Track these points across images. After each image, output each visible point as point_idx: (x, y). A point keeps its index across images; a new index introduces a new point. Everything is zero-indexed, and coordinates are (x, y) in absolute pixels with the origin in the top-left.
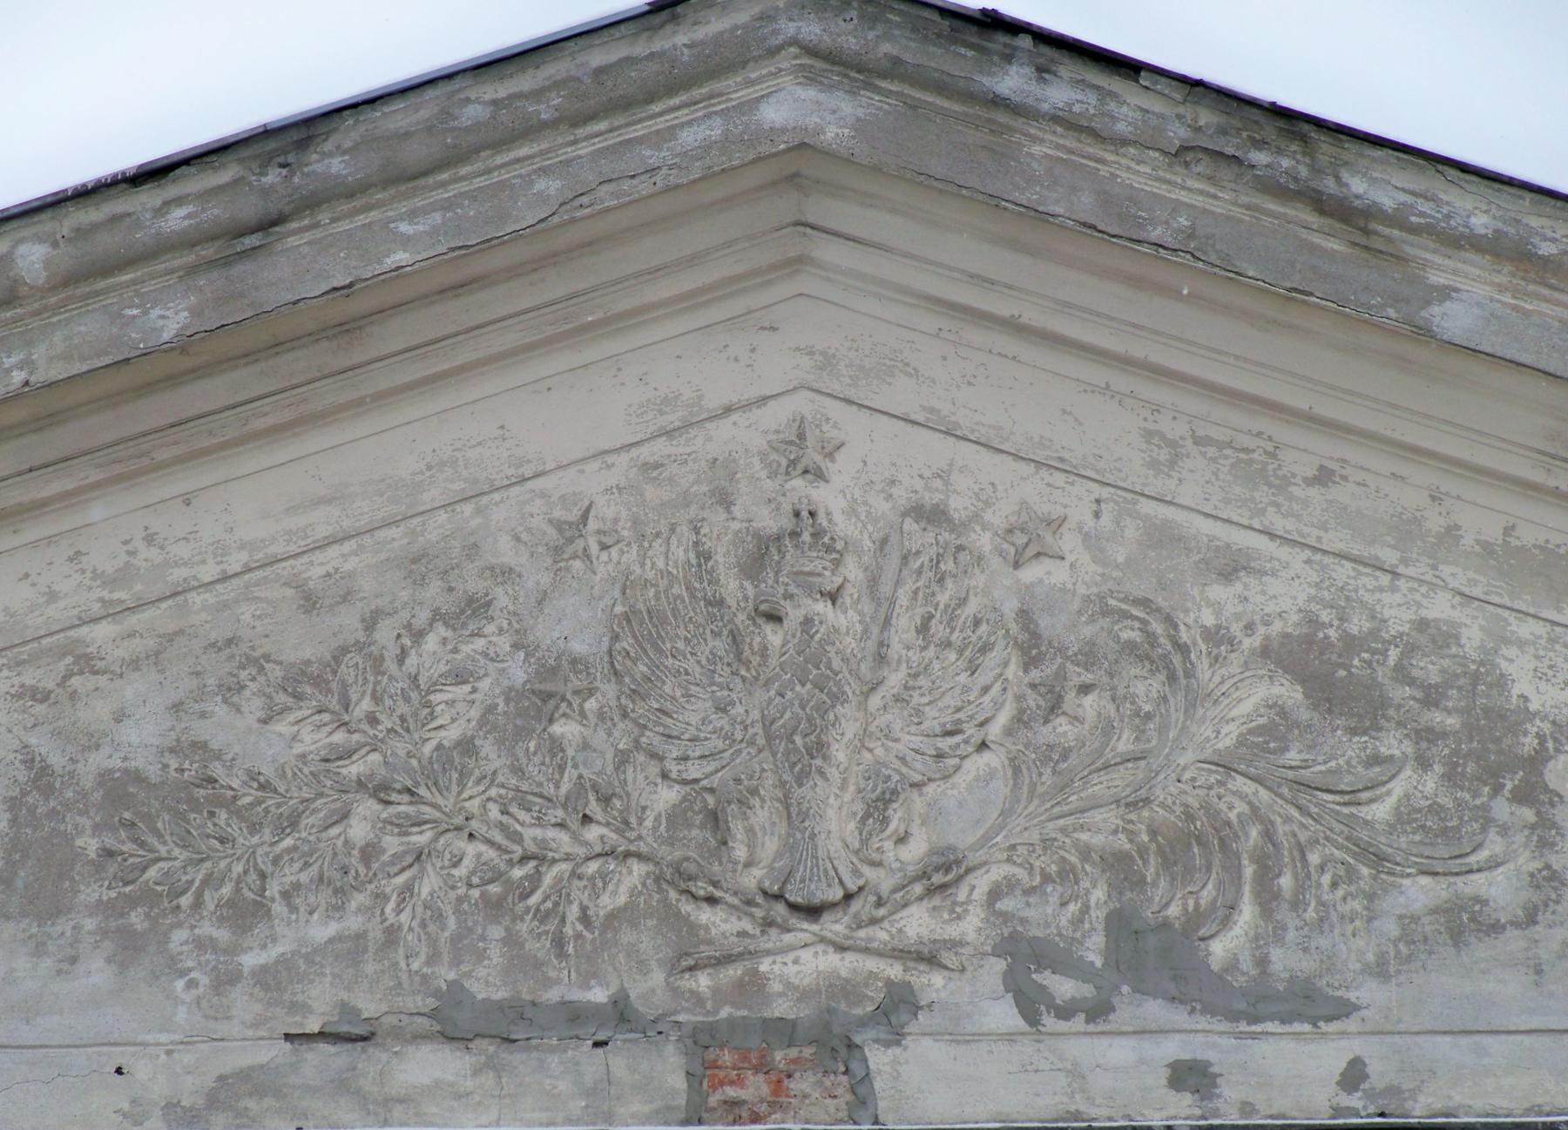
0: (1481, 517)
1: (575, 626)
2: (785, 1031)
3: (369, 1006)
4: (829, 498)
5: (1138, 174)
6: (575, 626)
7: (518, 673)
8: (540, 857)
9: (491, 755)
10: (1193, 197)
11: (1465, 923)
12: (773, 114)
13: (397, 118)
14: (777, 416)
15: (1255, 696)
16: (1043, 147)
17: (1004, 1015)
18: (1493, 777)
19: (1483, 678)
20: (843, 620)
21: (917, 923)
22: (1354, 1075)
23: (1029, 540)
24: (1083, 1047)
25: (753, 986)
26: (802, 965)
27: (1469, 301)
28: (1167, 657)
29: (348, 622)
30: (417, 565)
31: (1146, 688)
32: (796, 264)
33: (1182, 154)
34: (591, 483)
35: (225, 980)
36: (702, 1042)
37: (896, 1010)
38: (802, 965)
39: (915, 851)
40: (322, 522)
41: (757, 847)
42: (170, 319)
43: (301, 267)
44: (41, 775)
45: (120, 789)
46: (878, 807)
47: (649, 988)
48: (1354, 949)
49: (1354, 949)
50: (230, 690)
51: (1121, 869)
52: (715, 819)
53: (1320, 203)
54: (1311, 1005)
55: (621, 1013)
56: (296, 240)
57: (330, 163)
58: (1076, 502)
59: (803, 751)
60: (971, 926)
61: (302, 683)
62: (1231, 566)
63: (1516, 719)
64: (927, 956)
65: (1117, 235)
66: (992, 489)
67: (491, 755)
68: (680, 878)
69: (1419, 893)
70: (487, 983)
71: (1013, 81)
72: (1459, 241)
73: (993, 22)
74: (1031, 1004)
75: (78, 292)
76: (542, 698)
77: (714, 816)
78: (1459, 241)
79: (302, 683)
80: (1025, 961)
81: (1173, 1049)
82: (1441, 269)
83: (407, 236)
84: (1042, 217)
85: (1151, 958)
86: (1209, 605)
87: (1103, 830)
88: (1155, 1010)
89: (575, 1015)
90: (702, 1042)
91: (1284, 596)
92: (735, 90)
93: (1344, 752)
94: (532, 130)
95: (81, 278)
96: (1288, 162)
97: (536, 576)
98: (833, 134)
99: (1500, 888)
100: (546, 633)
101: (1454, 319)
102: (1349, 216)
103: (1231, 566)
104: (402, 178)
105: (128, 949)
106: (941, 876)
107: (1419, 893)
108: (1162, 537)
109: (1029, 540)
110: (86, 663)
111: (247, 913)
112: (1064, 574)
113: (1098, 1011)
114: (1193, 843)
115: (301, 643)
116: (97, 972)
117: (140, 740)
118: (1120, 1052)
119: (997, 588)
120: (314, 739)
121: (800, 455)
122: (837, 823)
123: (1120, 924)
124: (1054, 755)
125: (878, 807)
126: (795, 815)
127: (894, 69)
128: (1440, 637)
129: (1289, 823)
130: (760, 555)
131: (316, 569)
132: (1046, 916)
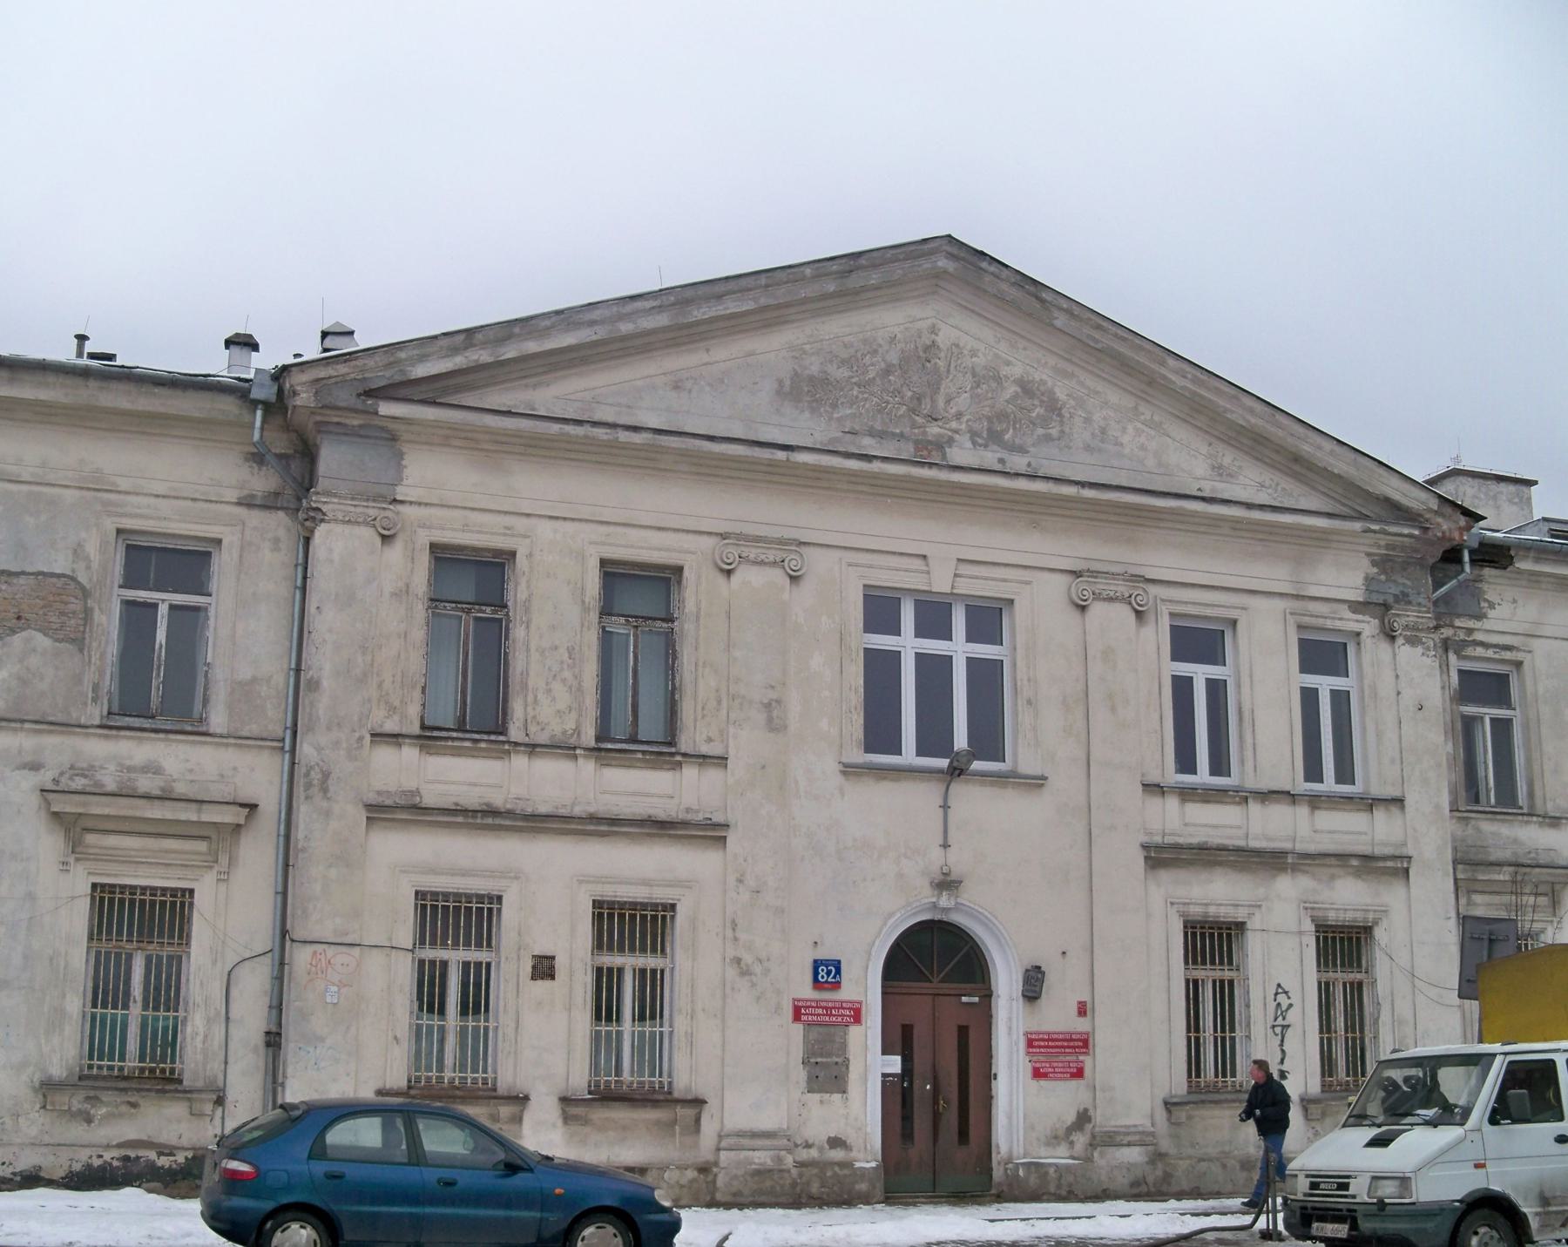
0: (1052, 361)
1: (893, 357)
2: (930, 442)
3: (857, 428)
4: (939, 339)
5: (1004, 286)
6: (893, 357)
7: (883, 365)
8: (887, 402)
9: (878, 381)
10: (1014, 293)
11: (1048, 438)
12: (940, 264)
13: (875, 254)
14: (929, 322)
15: (1012, 389)
16: (988, 278)
17: (969, 445)
18: (1053, 411)
19: (1051, 393)
20: (940, 363)
21: (954, 425)
22: (1029, 465)
23: (974, 353)
24: (982, 452)
25: (925, 433)
26: (934, 430)
27: (1061, 321)
28: (998, 379)
29: (852, 351)
30: (865, 341)
31: (994, 385)
32: (934, 293)
33: (1014, 284)
34: (896, 330)
35: (831, 419)
36: (916, 442)
37: (951, 441)
38: (934, 430)
39: (953, 411)
40: (848, 330)
41: (926, 407)
42: (831, 288)
43: (855, 281)
44: (796, 374)
45: (811, 379)
46: (948, 401)
47: (907, 430)
48: (1029, 441)
49: (1029, 441)
50: (831, 361)
51: (989, 419)
52: (919, 399)
53: (1037, 298)
54: (1022, 450)
55: (902, 435)
56: (854, 275)
57: (863, 261)
58: (982, 347)
59: (935, 387)
60: (963, 427)
61: (843, 362)
62: (1008, 363)
63: (1057, 400)
64: (956, 432)
65: (1000, 298)
66: (968, 343)
67: (878, 381)
68: (913, 411)
69: (1040, 431)
70: (878, 426)
71: (984, 265)
72: (1060, 309)
73: (982, 253)
74: (974, 443)
75: (1280, 433)
76: (887, 371)
77: (919, 399)
78: (1060, 309)
79: (843, 362)
80: (974, 435)
81: (999, 455)
82: (1056, 313)
83: (874, 278)
84: (985, 291)
85: (995, 437)
86: (1005, 371)
87: (986, 411)
88: (995, 447)
89: (894, 434)
90: (916, 442)
91: (1017, 371)
92: (933, 258)
93: (1028, 403)
94: (898, 260)
95: (817, 277)
96: (1032, 289)
97: (886, 347)
98: (951, 270)
99: (1054, 432)
100: (888, 358)
101: (1058, 323)
102: (1042, 301)
103: (1008, 363)
104: (874, 266)
105: (813, 411)
106: (959, 416)
107: (1040, 431)
108: (996, 355)
109: (974, 353)
110: (805, 352)
111: (834, 406)
112: (980, 361)
113: (986, 446)
114: (1002, 416)
115: (844, 354)
116: (807, 414)
117: (814, 369)
118: (990, 455)
119: (968, 361)
120: (846, 374)
121: (933, 330)
122: (941, 403)
123: (989, 430)
124: (978, 396)
125: (948, 401)
126: (933, 401)
127: (963, 259)
128: (1045, 383)
129: (1019, 415)
130: (927, 349)
131: (846, 339)
132: (976, 426)
